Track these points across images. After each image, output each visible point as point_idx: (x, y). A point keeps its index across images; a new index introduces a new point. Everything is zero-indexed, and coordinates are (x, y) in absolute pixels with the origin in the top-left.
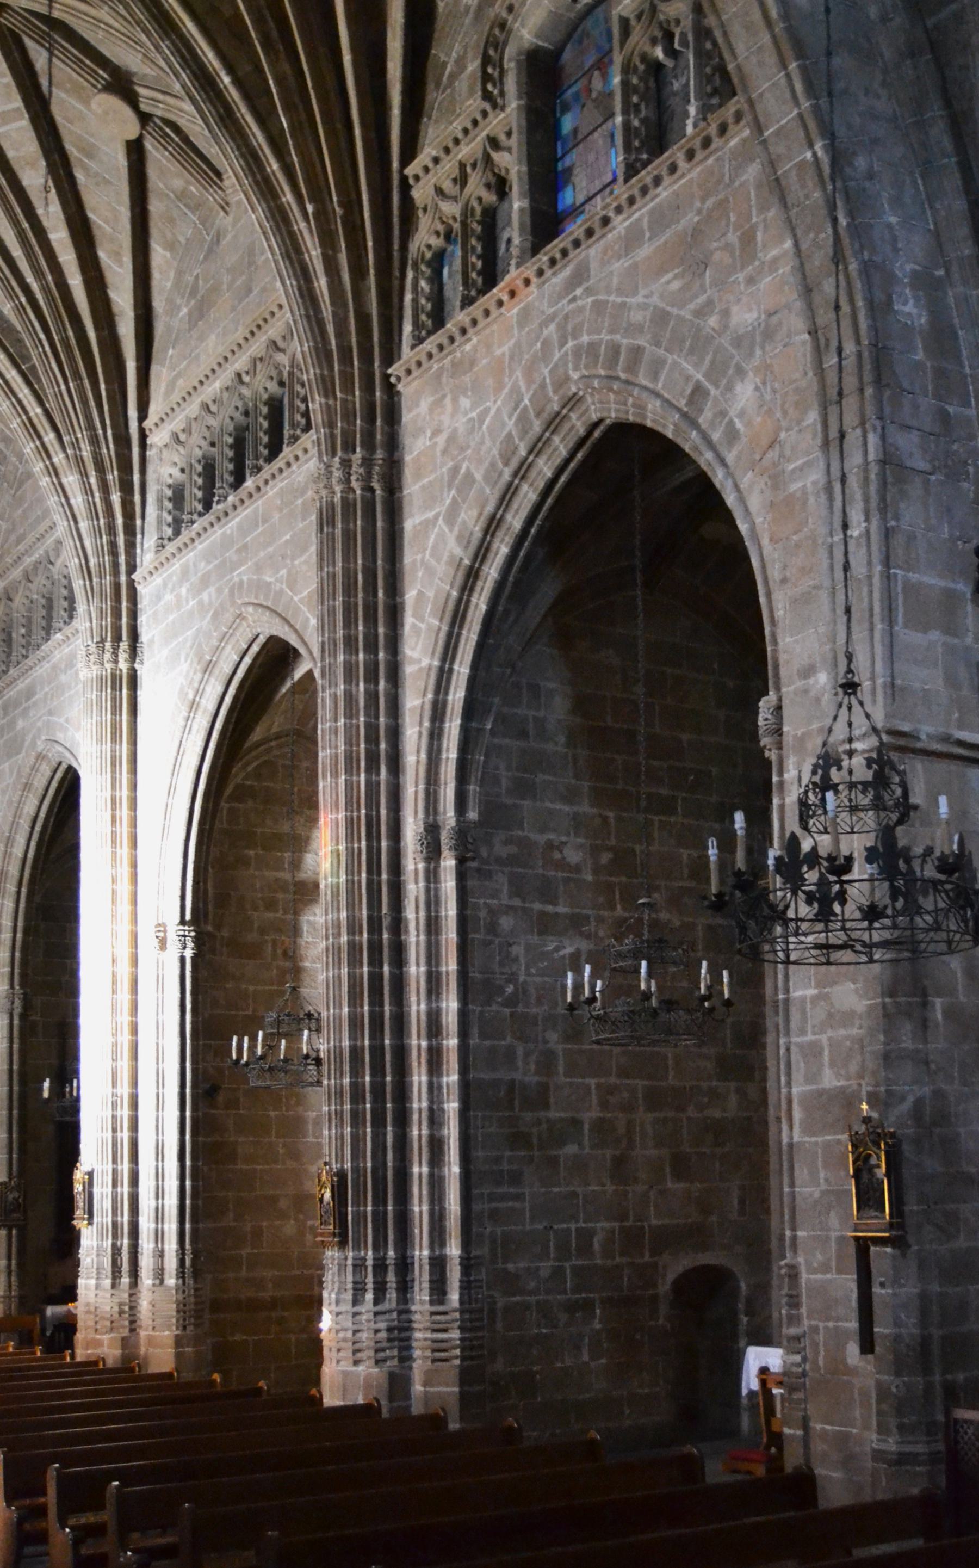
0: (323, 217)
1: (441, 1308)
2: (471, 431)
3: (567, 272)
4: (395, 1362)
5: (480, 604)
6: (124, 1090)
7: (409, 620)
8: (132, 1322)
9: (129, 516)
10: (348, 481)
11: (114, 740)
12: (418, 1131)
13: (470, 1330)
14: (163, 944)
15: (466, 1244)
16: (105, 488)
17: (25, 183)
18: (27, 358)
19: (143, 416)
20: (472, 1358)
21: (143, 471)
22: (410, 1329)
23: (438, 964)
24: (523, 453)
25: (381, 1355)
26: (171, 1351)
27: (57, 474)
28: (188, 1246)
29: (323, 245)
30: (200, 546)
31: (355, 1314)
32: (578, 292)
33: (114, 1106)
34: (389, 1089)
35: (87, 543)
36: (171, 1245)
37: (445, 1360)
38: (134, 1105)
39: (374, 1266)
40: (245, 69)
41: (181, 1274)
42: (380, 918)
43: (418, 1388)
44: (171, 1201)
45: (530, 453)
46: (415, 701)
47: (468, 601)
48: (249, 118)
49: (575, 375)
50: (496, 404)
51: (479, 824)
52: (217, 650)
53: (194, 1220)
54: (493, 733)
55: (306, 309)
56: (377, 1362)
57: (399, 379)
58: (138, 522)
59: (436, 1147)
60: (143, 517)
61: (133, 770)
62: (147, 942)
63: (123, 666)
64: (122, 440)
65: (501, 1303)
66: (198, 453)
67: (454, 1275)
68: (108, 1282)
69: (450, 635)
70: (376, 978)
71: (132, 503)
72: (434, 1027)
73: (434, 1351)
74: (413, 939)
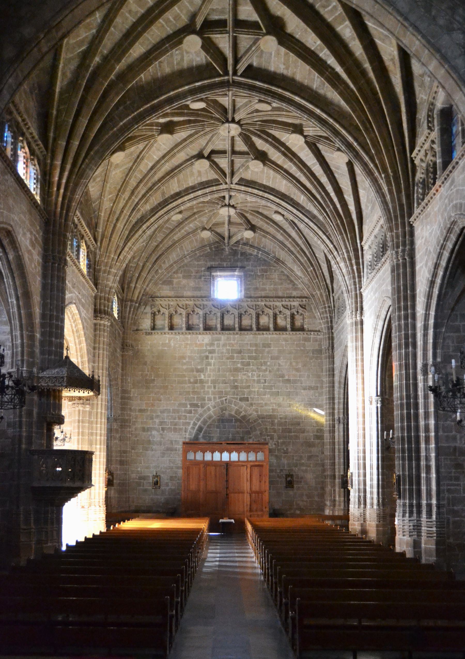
0: (387, 177)
1: (430, 520)
2: (430, 236)
3: (449, 182)
4: (416, 536)
5: (436, 291)
6: (361, 448)
7: (418, 299)
8: (364, 519)
9: (359, 272)
10: (398, 258)
11: (356, 341)
12: (423, 463)
13: (439, 528)
14: (371, 403)
15: (438, 499)
16: (352, 265)
17: (322, 181)
18: (328, 231)
19: (361, 239)
20: (441, 537)
21: (363, 258)
22: (421, 526)
23: (428, 409)
24: (442, 242)
25: (411, 534)
26: (375, 528)
27: (338, 264)
28: (380, 496)
29: (388, 186)
30: (375, 280)
31: (403, 520)
32: (452, 187)
33: (358, 453)
34: (413, 449)
35: (348, 283)
36: (375, 496)
37: (432, 537)
38: (364, 452)
39: (409, 505)
40: (361, 139)
41: (378, 505)
42: (410, 395)
43: (423, 545)
44: (375, 482)
45: (444, 241)
46: (420, 324)
47: (432, 291)
48: (363, 153)
49: (453, 215)
50: (435, 227)
51: (442, 362)
52: (380, 311)
53: (383, 488)
54: (446, 332)
55: (384, 207)
56: (410, 536)
57: (413, 222)
58: (362, 274)
59: (428, 468)
60: (363, 272)
61: (362, 350)
62: (367, 402)
63: (358, 318)
64: (356, 250)
65: (452, 520)
66: (375, 251)
67: (434, 509)
68: (357, 506)
69: (427, 303)
70: (409, 414)
71: (360, 268)
72: (427, 429)
73: (427, 534)
74: (420, 401)
